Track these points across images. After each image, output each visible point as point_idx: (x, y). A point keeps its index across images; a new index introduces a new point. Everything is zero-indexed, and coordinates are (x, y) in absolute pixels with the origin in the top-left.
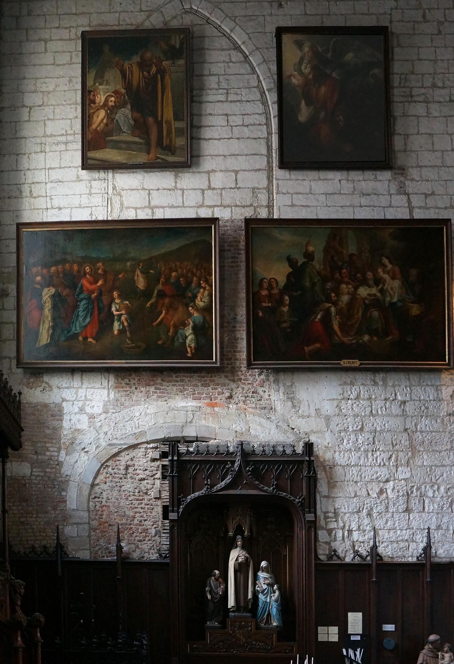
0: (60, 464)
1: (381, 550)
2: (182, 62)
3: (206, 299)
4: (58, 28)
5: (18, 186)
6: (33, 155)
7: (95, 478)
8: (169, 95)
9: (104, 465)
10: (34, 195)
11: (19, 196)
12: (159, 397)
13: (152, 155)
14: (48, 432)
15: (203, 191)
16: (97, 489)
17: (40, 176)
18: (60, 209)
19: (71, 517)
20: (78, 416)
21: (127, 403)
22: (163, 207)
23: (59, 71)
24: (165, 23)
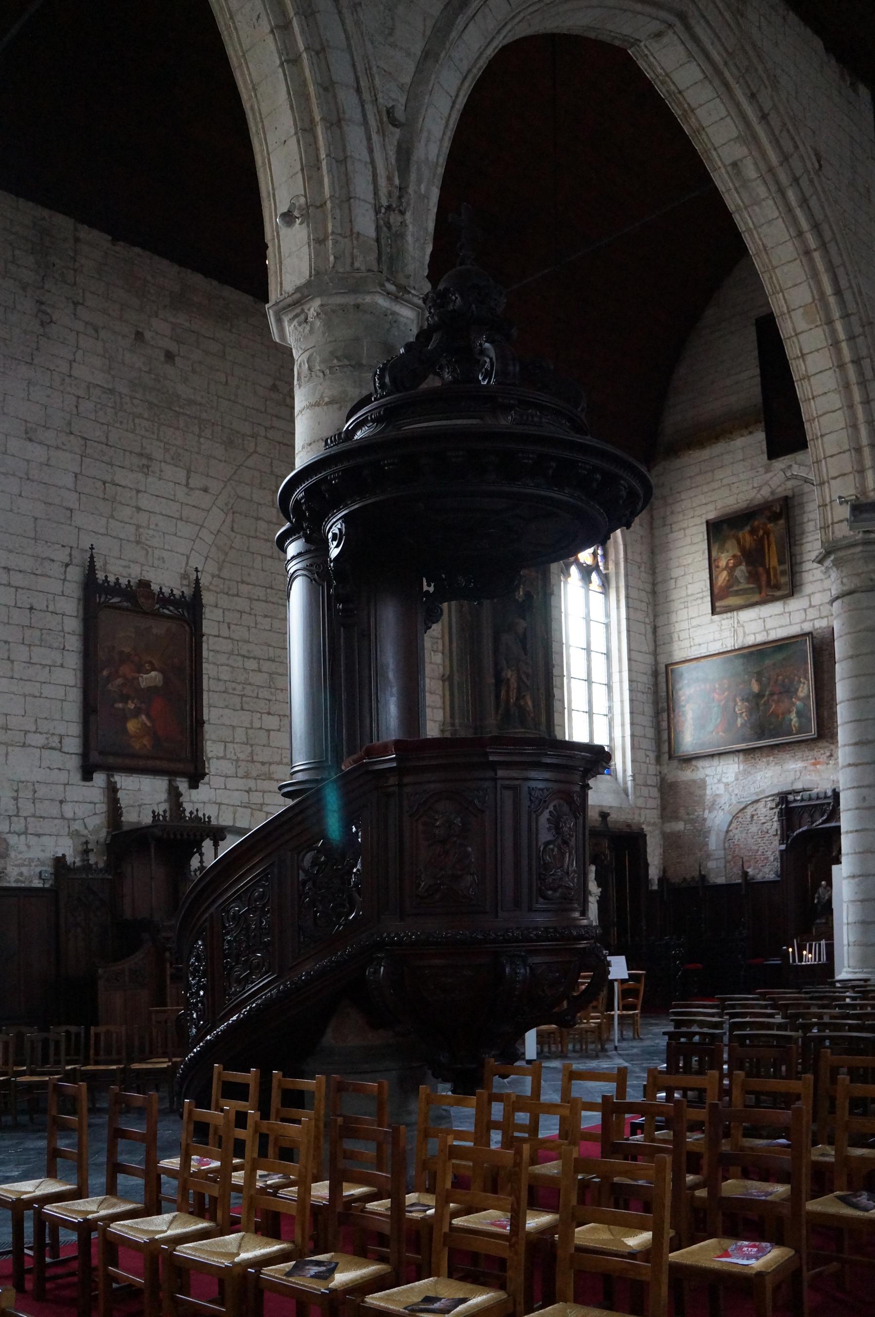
0: (705, 820)
1: (750, 871)
3: (806, 691)
5: (670, 635)
6: (680, 612)
8: (774, 547)
9: (735, 817)
11: (670, 642)
12: (776, 764)
13: (763, 594)
15: (805, 610)
17: (685, 625)
20: (717, 785)
21: (752, 771)
22: (775, 628)
23: (694, 548)
24: (772, 493)
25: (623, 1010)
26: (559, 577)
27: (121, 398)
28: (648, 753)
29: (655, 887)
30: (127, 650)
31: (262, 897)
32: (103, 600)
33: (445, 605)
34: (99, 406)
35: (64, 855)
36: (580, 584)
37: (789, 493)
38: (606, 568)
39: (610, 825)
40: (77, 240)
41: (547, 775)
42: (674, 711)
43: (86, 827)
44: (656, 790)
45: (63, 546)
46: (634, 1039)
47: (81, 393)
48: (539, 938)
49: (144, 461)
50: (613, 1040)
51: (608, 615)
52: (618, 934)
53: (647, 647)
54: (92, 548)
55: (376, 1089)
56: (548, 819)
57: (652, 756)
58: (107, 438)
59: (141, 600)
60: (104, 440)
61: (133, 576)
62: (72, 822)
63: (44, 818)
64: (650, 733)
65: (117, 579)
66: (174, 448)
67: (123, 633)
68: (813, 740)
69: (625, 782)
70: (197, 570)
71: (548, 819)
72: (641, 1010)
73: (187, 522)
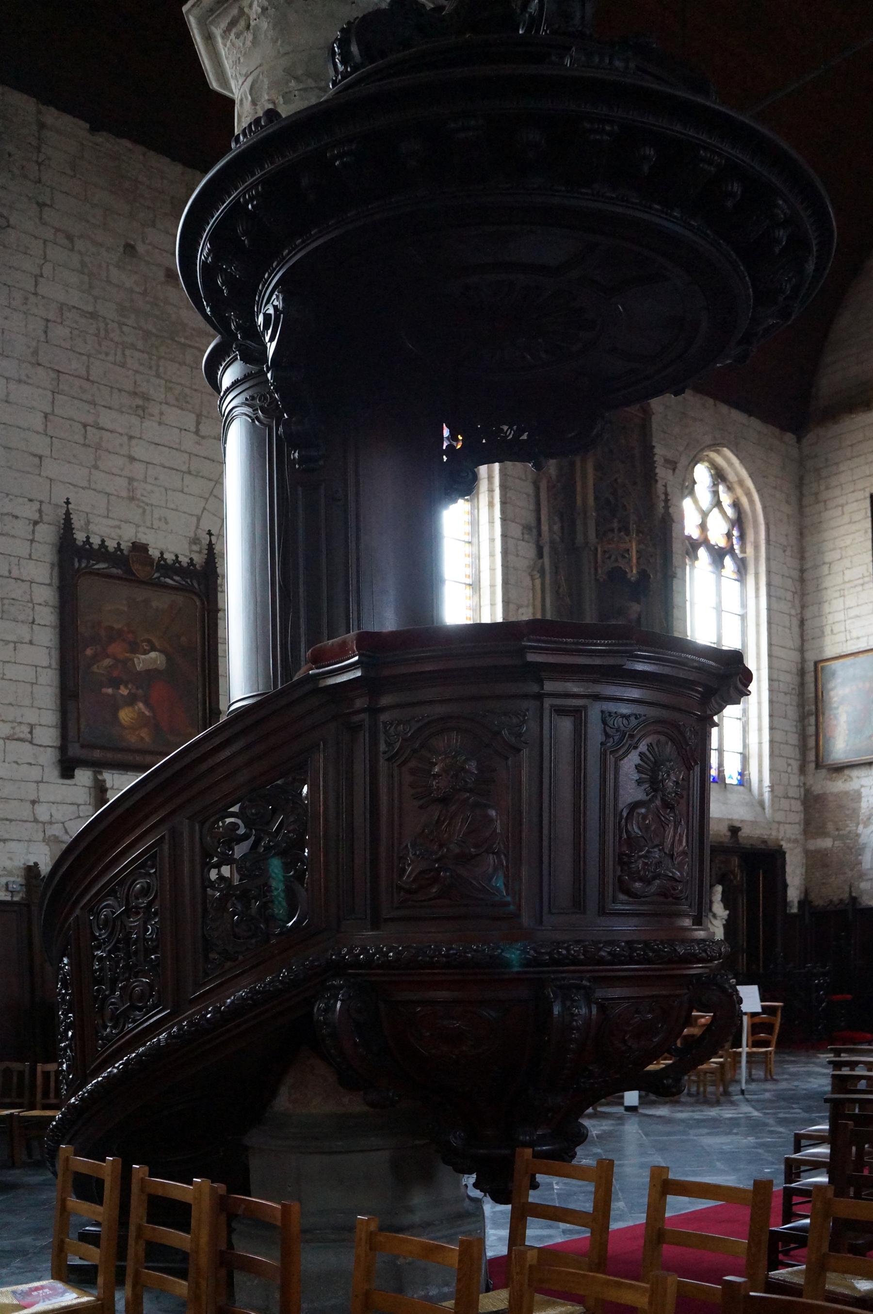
0: (858, 835)
4: (853, 492)
10: (835, 632)
11: (822, 634)
14: (847, 812)
19: (865, 875)
23: (855, 527)
25: (754, 1046)
26: (684, 558)
27: (107, 324)
28: (790, 761)
29: (795, 910)
30: (117, 626)
31: (145, 892)
32: (79, 563)
33: (483, 469)
34: (76, 332)
35: (36, 864)
36: (710, 568)
38: (743, 551)
39: (741, 840)
40: (42, 126)
41: (635, 693)
42: (823, 714)
43: (66, 832)
44: (799, 803)
45: (31, 500)
46: (766, 1080)
47: (51, 316)
48: (616, 959)
49: (140, 402)
50: (738, 1082)
51: (744, 605)
52: (750, 953)
53: (792, 642)
54: (68, 503)
55: (279, 1215)
56: (637, 766)
57: (795, 765)
58: (88, 372)
59: (135, 567)
60: (83, 372)
61: (126, 539)
62: (47, 827)
63: (11, 821)
64: (793, 739)
65: (103, 541)
66: (179, 387)
67: (113, 605)
69: (761, 794)
70: (210, 533)
71: (637, 766)
72: (776, 1047)
73: (196, 476)
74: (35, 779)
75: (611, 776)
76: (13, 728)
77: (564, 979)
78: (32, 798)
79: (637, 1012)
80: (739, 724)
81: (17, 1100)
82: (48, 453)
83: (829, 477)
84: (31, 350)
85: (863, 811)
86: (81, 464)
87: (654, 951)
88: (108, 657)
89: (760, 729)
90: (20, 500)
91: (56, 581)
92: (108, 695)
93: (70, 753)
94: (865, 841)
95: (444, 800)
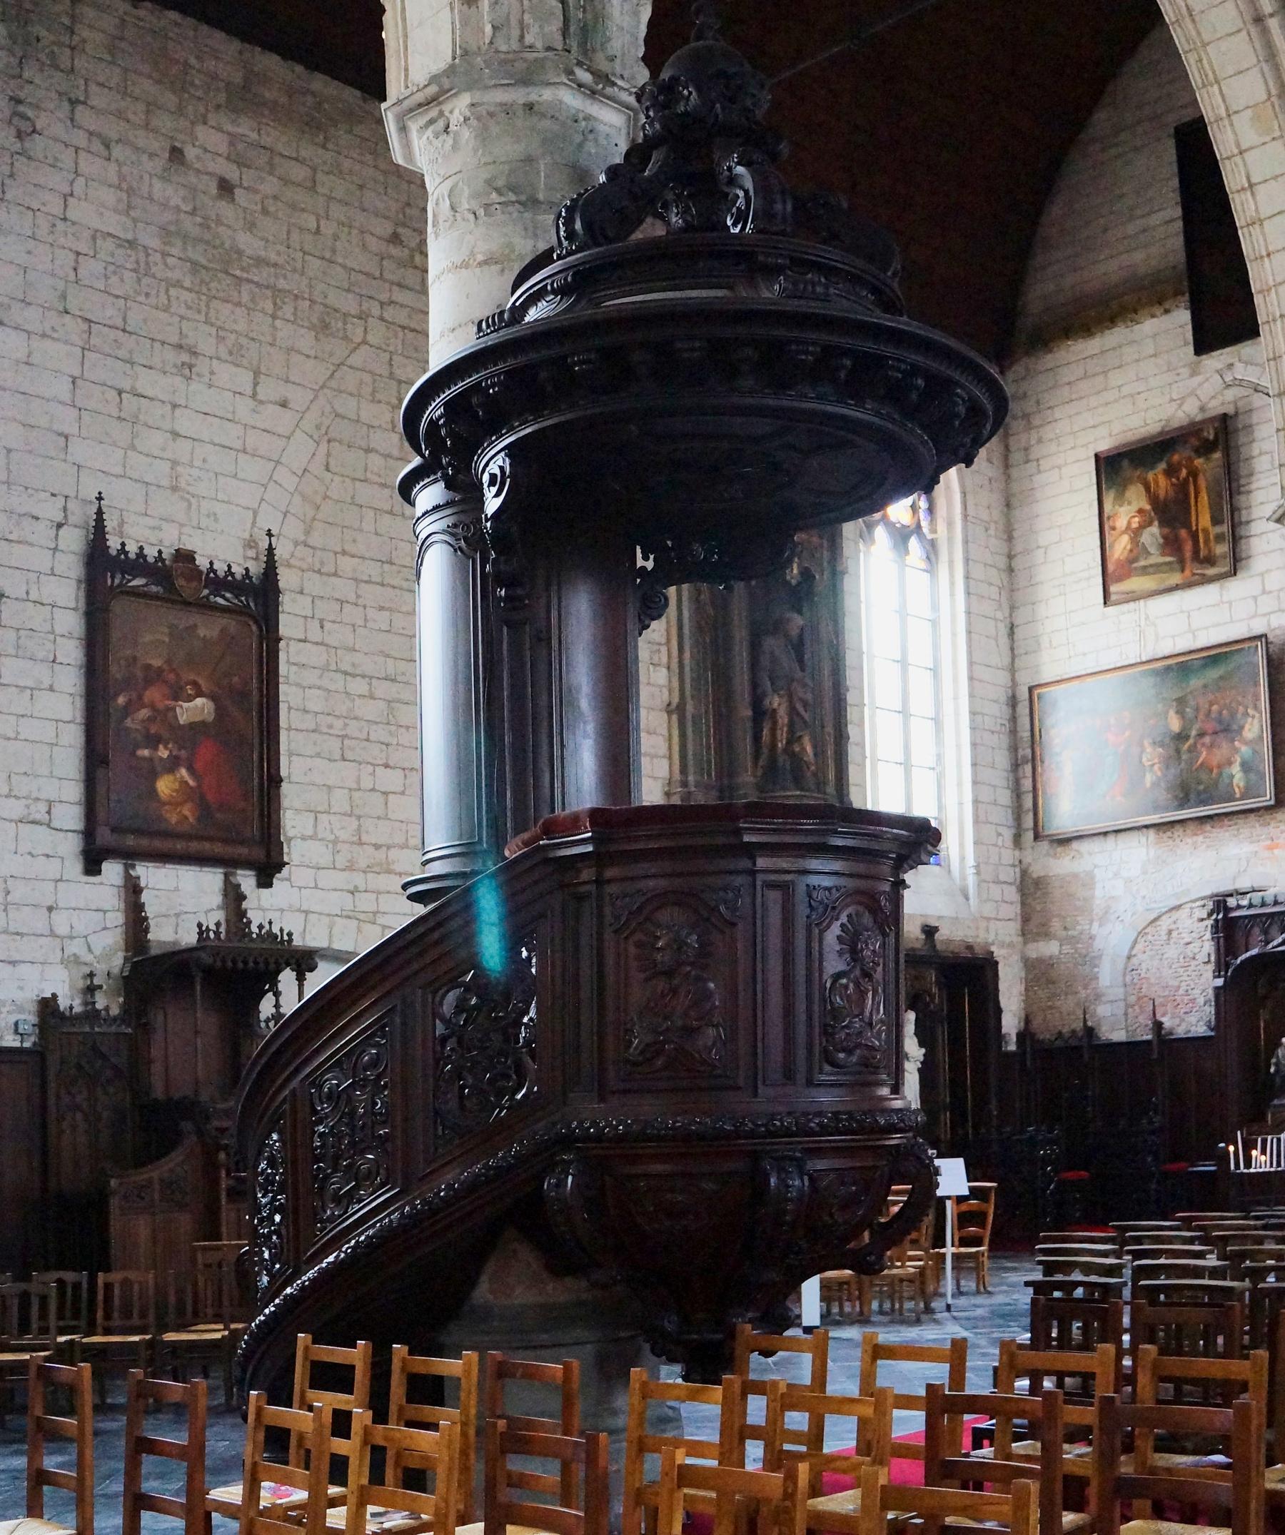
2: (1217, 455)
7: (1133, 948)
8: (1204, 497)
13: (1187, 572)
15: (1255, 598)
16: (1135, 961)
18: (1085, 654)
19: (1103, 995)
22: (1206, 628)
24: (1202, 409)
25: (961, 1245)
26: (857, 543)
27: (148, 255)
28: (1001, 829)
29: (1012, 1047)
30: (157, 663)
31: (374, 1063)
32: (116, 581)
33: (672, 590)
34: (111, 268)
35: (54, 996)
37: (1230, 410)
38: (934, 531)
39: (939, 947)
41: (837, 866)
44: (1013, 889)
45: (53, 495)
47: (83, 248)
48: (824, 1130)
49: (185, 357)
50: (943, 1295)
51: (935, 607)
54: (100, 499)
56: (839, 937)
57: (1008, 834)
58: (124, 319)
59: (180, 582)
60: (119, 323)
61: (167, 543)
64: (1005, 797)
65: (141, 548)
66: (233, 336)
67: (150, 635)
68: (1267, 808)
69: (963, 878)
70: (269, 534)
71: (839, 937)
72: (990, 1245)
73: (254, 455)
74: (51, 876)
75: (816, 945)
76: (28, 807)
77: (777, 1151)
78: (49, 904)
79: (843, 1183)
80: (932, 776)
81: (73, 1323)
82: (76, 431)
83: (1041, 426)
84: (59, 293)
85: (1098, 902)
86: (114, 444)
87: (857, 1121)
88: (143, 706)
89: (960, 784)
90: (43, 495)
91: (82, 604)
92: (144, 758)
93: (99, 841)
94: (1101, 947)
95: (669, 974)
